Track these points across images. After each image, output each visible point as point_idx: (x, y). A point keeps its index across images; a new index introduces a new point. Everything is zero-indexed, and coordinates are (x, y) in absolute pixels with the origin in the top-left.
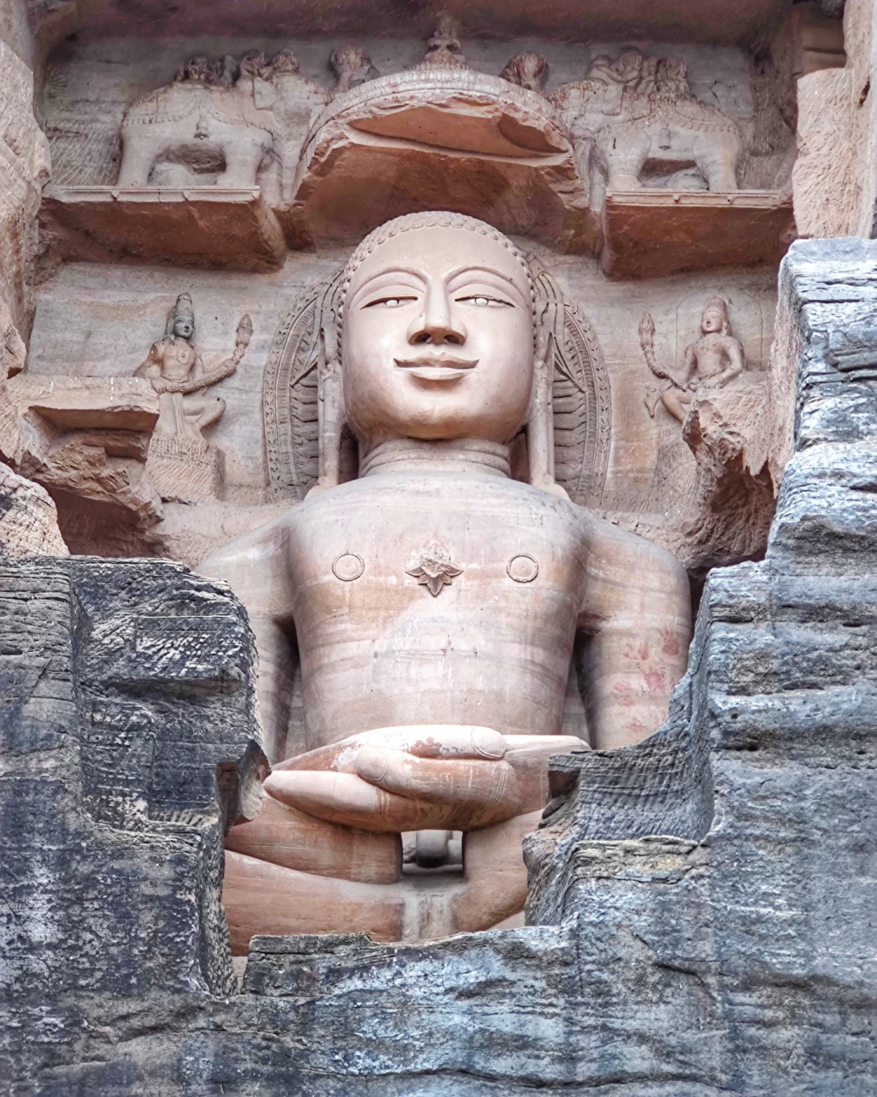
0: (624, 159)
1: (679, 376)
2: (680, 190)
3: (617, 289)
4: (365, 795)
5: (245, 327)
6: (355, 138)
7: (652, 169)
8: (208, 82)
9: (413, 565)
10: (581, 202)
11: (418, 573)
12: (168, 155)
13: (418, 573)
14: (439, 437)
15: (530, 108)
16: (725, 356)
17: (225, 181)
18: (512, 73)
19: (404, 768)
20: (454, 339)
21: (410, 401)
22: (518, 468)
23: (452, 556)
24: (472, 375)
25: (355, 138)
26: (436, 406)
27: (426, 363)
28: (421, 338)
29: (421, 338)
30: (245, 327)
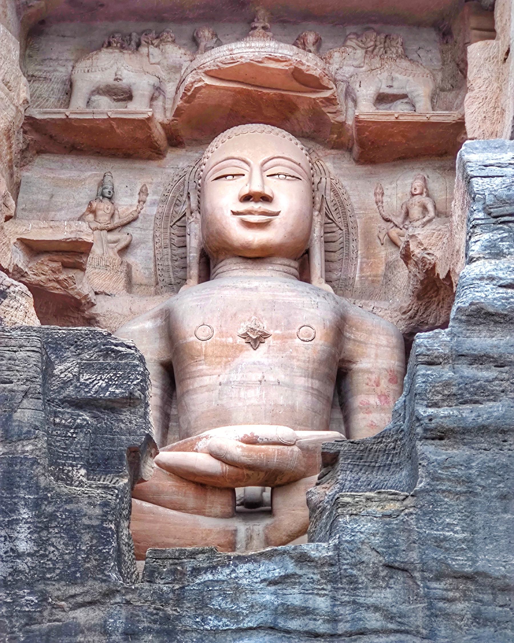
0: (366, 93)
1: (398, 220)
2: (399, 111)
3: (361, 170)
4: (214, 466)
5: (143, 192)
6: (208, 81)
7: (382, 99)
8: (122, 48)
9: (242, 331)
10: (340, 118)
11: (245, 336)
12: (99, 91)
13: (245, 336)
14: (257, 257)
15: (311, 63)
16: (425, 208)
17: (132, 106)
18: (300, 43)
19: (236, 450)
20: (266, 199)
21: (240, 235)
22: (304, 274)
23: (265, 326)
24: (277, 220)
25: (208, 81)
26: (256, 238)
27: (250, 213)
28: (247, 198)
29: (247, 198)
30: (143, 192)
